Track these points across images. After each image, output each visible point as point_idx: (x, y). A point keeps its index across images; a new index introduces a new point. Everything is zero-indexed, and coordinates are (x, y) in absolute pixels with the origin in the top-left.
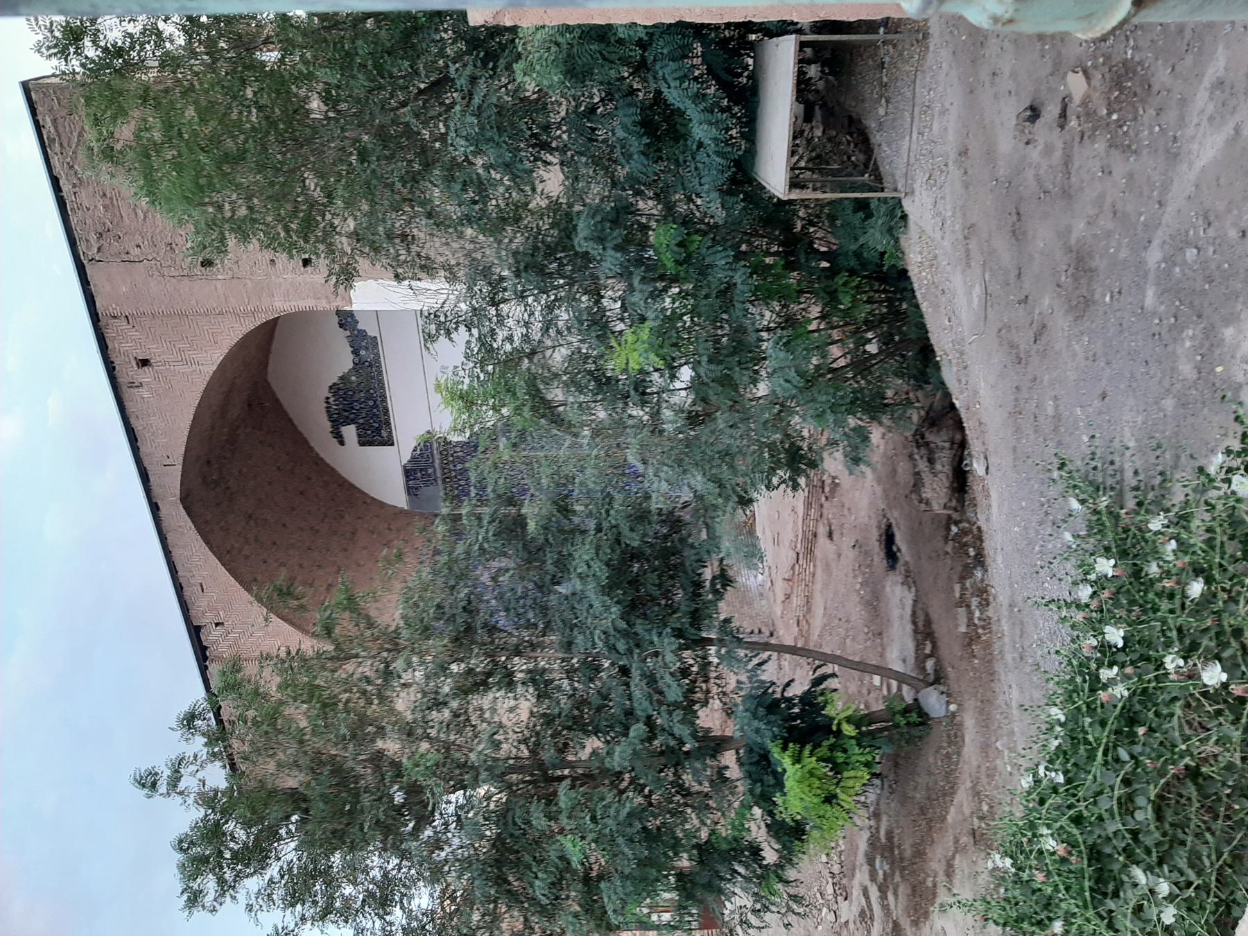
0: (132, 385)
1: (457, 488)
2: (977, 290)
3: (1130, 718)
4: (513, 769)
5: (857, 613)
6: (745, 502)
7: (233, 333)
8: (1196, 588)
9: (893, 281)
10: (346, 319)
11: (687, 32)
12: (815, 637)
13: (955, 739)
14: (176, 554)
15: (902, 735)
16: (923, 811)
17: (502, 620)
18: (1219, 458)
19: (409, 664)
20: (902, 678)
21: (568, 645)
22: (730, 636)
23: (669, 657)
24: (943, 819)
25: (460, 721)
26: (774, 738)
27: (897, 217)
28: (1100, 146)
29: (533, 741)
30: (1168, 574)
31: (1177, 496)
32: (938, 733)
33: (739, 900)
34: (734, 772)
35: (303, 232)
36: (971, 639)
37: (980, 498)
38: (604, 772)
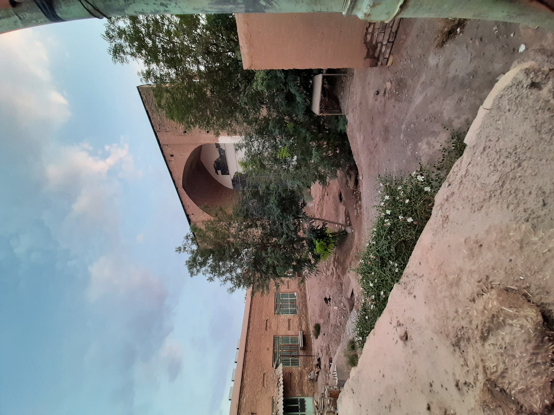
0: (170, 161)
1: (243, 183)
2: (362, 137)
3: (391, 230)
4: (258, 244)
5: (333, 212)
6: (309, 187)
7: (192, 149)
8: (407, 201)
9: (343, 136)
10: (218, 146)
11: (297, 72)
12: (324, 216)
13: (353, 238)
14: (182, 199)
15: (342, 237)
16: (345, 253)
17: (254, 213)
18: (415, 173)
19: (234, 222)
20: (342, 225)
21: (269, 218)
22: (305, 217)
23: (291, 221)
24: (349, 254)
25: (246, 234)
26: (314, 237)
27: (346, 122)
28: (393, 100)
29: (262, 238)
30: (401, 199)
31: (405, 181)
32: (350, 237)
33: (306, 271)
34: (305, 245)
35: (207, 124)
36: (357, 216)
37: (361, 186)
38: (277, 245)
